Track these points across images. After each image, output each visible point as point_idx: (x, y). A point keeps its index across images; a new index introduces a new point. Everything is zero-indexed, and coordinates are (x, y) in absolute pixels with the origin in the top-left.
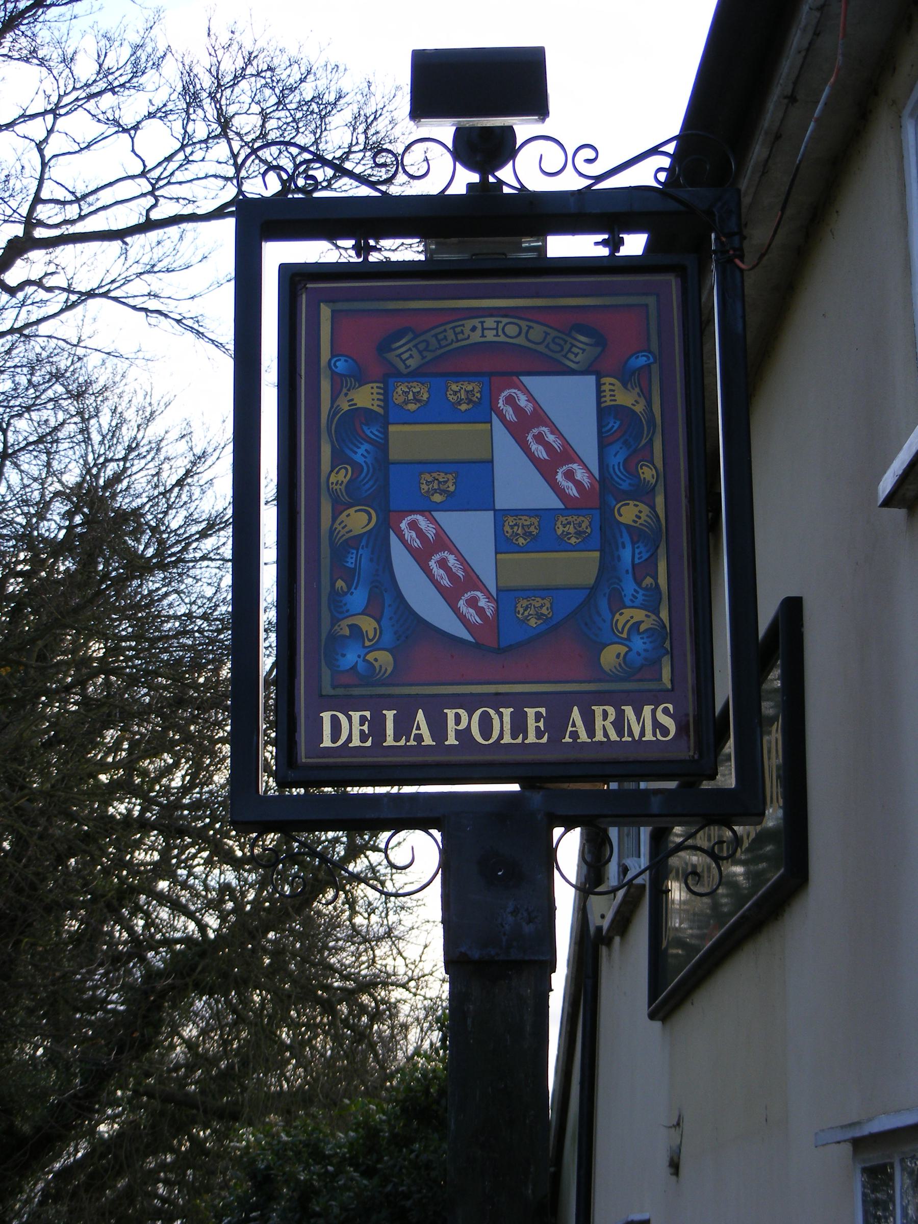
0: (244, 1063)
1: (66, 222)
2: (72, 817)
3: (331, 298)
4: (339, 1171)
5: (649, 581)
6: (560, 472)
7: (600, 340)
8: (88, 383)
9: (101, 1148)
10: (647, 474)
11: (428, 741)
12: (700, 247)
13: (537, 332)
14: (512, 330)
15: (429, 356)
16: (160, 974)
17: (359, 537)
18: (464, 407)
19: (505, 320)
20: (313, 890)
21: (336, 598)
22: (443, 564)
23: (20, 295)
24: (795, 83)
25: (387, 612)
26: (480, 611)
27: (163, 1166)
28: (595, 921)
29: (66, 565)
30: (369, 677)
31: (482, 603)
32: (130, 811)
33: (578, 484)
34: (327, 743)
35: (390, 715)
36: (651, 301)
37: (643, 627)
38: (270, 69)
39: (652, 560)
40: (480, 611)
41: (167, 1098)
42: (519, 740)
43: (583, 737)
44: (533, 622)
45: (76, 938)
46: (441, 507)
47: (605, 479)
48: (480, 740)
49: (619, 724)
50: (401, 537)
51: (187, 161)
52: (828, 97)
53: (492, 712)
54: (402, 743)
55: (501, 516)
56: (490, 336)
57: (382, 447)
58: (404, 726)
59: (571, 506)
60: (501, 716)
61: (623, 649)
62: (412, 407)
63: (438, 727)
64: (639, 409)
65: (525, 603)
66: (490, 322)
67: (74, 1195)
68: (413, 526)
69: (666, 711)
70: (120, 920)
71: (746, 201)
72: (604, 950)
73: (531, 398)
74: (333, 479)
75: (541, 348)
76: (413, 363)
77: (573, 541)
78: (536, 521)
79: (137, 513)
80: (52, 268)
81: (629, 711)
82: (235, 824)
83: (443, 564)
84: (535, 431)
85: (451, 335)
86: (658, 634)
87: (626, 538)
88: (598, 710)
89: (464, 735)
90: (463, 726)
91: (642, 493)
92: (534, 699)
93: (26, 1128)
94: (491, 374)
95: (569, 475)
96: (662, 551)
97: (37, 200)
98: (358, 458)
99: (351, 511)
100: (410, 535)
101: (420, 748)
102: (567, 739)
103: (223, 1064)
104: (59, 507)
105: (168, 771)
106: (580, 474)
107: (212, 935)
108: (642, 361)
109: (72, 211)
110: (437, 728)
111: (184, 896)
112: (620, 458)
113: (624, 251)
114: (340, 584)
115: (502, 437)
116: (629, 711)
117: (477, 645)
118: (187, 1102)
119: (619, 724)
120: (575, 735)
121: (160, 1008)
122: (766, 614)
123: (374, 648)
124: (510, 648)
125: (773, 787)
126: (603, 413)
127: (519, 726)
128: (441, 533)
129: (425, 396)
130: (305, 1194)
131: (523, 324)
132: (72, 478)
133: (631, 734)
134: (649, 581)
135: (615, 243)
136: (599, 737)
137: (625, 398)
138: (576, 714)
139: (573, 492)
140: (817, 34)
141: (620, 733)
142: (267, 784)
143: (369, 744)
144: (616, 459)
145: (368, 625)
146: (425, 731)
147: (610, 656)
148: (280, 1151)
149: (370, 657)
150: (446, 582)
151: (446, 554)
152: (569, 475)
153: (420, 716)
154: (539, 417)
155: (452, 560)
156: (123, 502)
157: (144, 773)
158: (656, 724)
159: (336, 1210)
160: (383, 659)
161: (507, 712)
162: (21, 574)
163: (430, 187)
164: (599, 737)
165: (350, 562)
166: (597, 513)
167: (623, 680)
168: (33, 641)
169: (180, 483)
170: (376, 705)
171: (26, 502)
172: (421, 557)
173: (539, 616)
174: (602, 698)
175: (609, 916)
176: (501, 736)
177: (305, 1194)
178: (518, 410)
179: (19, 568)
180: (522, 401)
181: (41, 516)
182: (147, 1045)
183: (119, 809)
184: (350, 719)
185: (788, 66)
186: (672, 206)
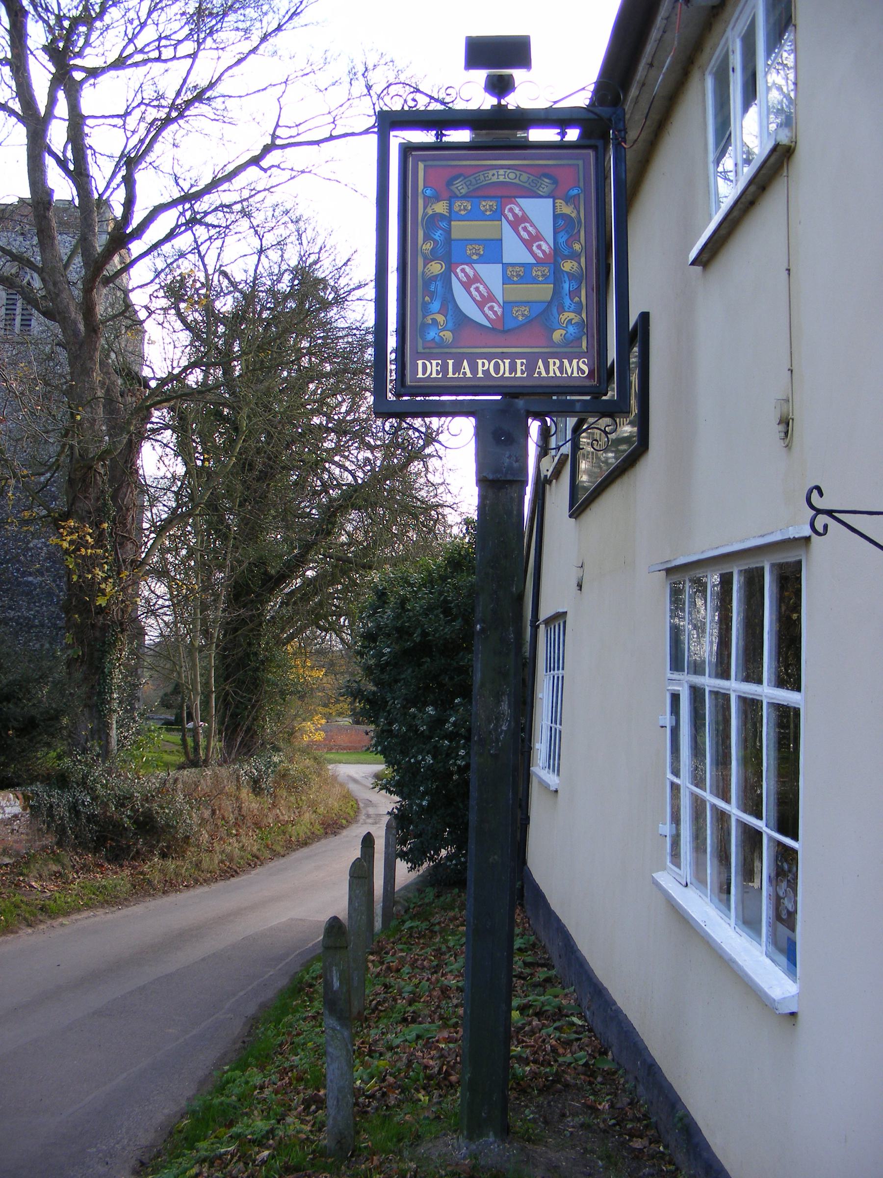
0: (375, 542)
1: (291, 137)
2: (295, 426)
3: (424, 159)
4: (419, 589)
5: (577, 299)
6: (535, 245)
7: (555, 182)
8: (301, 216)
9: (308, 582)
10: (577, 247)
11: (469, 375)
12: (605, 137)
13: (524, 177)
14: (512, 176)
15: (472, 188)
16: (335, 500)
17: (437, 276)
18: (488, 213)
19: (509, 171)
20: (409, 460)
21: (425, 305)
22: (477, 289)
23: (269, 172)
24: (653, 57)
25: (450, 313)
26: (495, 313)
27: (337, 591)
28: (544, 472)
29: (291, 304)
30: (441, 344)
31: (496, 308)
32: (321, 423)
33: (543, 252)
34: (420, 375)
35: (451, 362)
36: (580, 163)
37: (573, 322)
38: (392, 61)
39: (579, 289)
40: (495, 313)
41: (339, 559)
42: (513, 375)
43: (544, 374)
44: (520, 318)
45: (296, 483)
46: (476, 262)
47: (556, 249)
48: (494, 375)
49: (561, 368)
50: (457, 276)
51: (351, 106)
52: (670, 64)
53: (500, 361)
54: (456, 376)
55: (505, 266)
56: (501, 179)
57: (448, 232)
58: (457, 368)
59: (539, 262)
60: (504, 363)
61: (564, 332)
62: (463, 213)
63: (474, 368)
64: (573, 215)
65: (516, 309)
66: (501, 172)
67: (295, 603)
68: (463, 271)
69: (584, 362)
70: (316, 475)
71: (627, 116)
72: (548, 486)
73: (521, 209)
74: (424, 247)
75: (526, 185)
76: (464, 191)
77: (540, 279)
78: (522, 269)
79: (324, 280)
80: (284, 159)
81: (566, 362)
82: (375, 413)
83: (477, 289)
84: (523, 225)
85: (482, 178)
86: (581, 325)
87: (566, 279)
88: (551, 361)
89: (486, 372)
90: (485, 368)
91: (574, 256)
92: (520, 356)
93: (273, 572)
94: (501, 197)
95: (539, 247)
96: (583, 285)
97: (277, 126)
98: (437, 237)
99: (433, 263)
100: (461, 275)
101: (465, 378)
102: (536, 375)
103: (365, 544)
104: (287, 277)
105: (340, 404)
106: (545, 247)
107: (360, 481)
108: (575, 192)
109: (294, 132)
110: (474, 369)
111: (347, 464)
112: (564, 239)
113: (567, 138)
114: (427, 298)
115: (507, 228)
116: (566, 362)
117: (493, 329)
118: (348, 561)
119: (561, 368)
120: (539, 373)
121: (335, 516)
122: (633, 319)
123: (442, 330)
124: (509, 330)
125: (633, 402)
126: (556, 217)
127: (513, 369)
128: (476, 274)
129: (469, 208)
130: (403, 601)
131: (518, 173)
132: (293, 262)
133: (567, 373)
134: (577, 299)
135: (563, 134)
136: (551, 374)
137: (567, 210)
138: (540, 363)
139: (541, 255)
140: (664, 32)
141: (561, 373)
142: (391, 397)
143: (440, 376)
144: (562, 240)
145: (440, 319)
146: (467, 370)
147: (557, 336)
148: (390, 581)
149: (441, 334)
150: (478, 298)
151: (478, 285)
152: (539, 247)
153: (465, 363)
154: (525, 219)
155: (481, 288)
156: (320, 275)
157: (328, 405)
158: (579, 368)
159: (418, 609)
160: (448, 335)
161: (507, 361)
162: (269, 309)
163: (473, 106)
164: (551, 374)
165: (432, 288)
166: (552, 266)
167: (563, 347)
168: (275, 340)
169: (345, 264)
170: (444, 357)
171: (272, 274)
172: (467, 286)
173: (523, 315)
174: (554, 355)
175: (551, 470)
176: (504, 373)
177: (403, 601)
178: (515, 215)
179: (269, 305)
180: (517, 210)
181: (279, 281)
182: (329, 533)
183: (316, 420)
184: (431, 364)
185: (649, 48)
186: (592, 116)
